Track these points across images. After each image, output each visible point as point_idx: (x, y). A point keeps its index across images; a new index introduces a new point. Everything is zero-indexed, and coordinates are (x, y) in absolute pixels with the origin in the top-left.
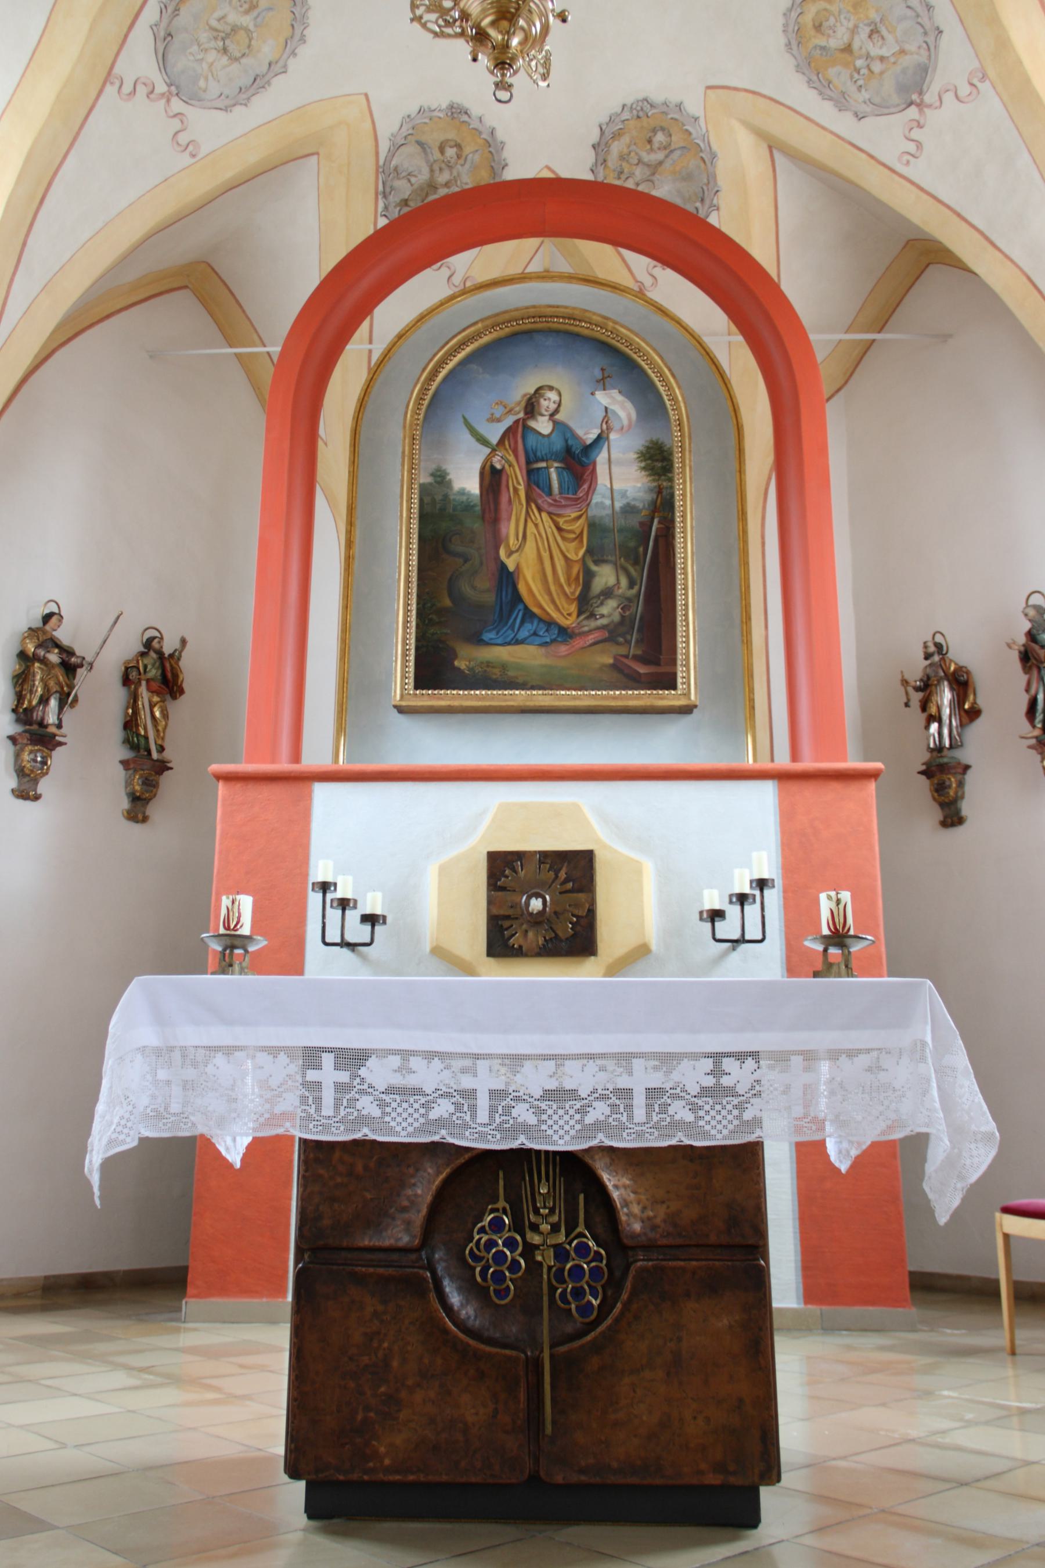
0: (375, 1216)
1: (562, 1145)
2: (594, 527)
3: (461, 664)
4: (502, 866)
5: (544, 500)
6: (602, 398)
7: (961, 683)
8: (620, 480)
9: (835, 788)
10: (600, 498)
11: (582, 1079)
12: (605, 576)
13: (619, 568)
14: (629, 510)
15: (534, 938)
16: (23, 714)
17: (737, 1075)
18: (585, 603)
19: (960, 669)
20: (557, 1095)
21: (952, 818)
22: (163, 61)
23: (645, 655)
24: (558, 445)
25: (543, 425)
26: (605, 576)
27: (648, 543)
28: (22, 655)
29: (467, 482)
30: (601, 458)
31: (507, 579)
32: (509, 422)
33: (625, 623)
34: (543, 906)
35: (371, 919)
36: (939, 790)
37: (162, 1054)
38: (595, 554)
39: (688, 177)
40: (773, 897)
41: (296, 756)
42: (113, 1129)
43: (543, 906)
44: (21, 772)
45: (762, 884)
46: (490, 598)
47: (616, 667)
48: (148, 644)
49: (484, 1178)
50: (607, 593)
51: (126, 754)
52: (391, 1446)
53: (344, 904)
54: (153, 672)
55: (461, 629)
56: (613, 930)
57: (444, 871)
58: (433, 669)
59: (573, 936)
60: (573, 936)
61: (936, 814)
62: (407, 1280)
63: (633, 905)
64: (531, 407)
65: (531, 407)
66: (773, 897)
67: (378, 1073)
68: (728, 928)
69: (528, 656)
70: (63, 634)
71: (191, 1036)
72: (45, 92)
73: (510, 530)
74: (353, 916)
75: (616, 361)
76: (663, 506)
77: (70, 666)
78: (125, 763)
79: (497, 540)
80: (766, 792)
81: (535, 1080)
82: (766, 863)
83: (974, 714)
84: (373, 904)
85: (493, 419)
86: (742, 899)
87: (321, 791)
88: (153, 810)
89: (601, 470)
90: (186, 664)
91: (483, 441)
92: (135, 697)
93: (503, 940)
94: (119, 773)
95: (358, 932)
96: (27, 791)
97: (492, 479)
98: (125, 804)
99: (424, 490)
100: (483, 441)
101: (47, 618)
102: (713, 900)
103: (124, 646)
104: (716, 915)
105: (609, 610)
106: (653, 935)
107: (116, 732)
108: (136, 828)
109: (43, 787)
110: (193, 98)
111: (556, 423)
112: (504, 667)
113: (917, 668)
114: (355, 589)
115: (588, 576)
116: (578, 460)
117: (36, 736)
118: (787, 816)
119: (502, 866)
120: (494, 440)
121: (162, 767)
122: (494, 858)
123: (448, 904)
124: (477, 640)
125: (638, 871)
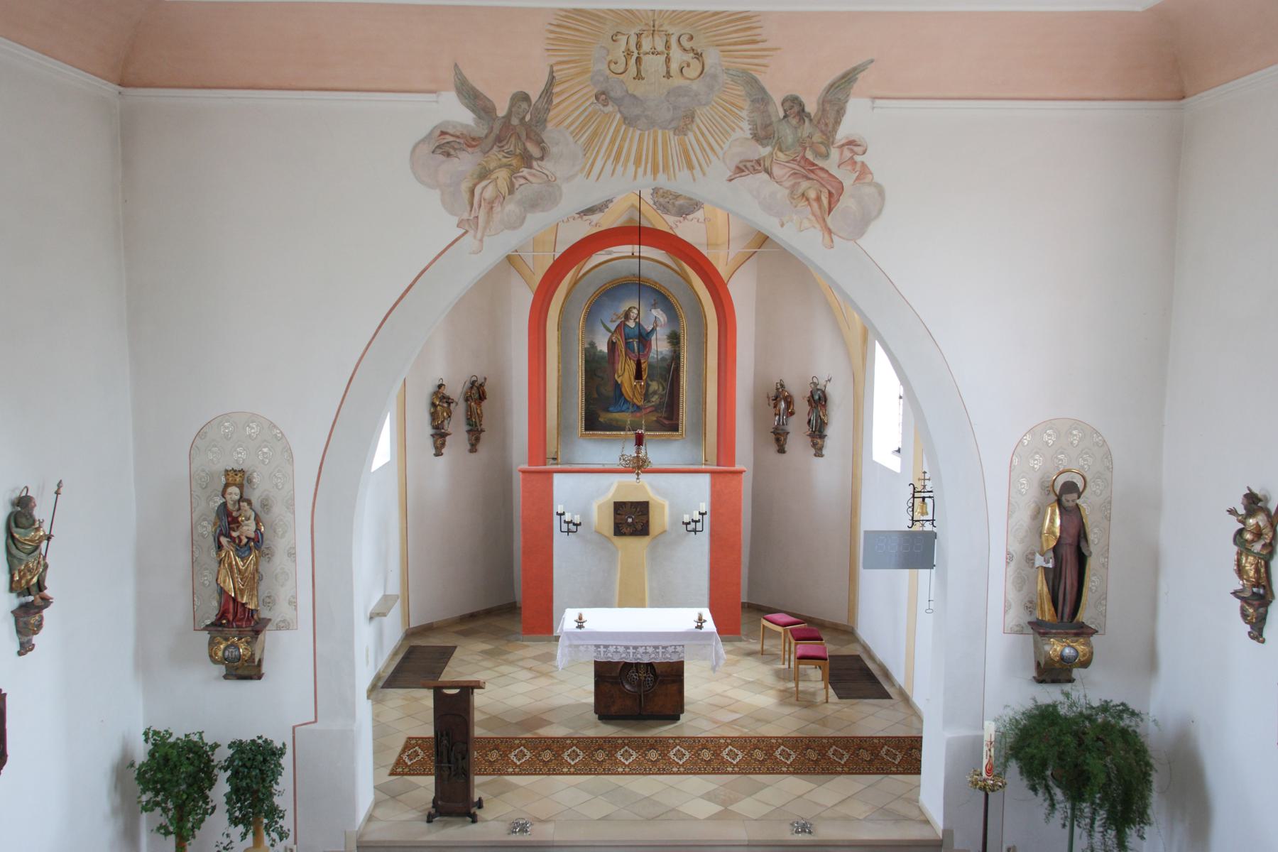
1: (646, 660)
3: (601, 420)
4: (619, 507)
6: (654, 312)
7: (789, 401)
8: (660, 347)
10: (653, 354)
12: (654, 386)
13: (659, 383)
14: (663, 359)
15: (629, 530)
17: (679, 649)
18: (646, 396)
19: (790, 396)
21: (781, 450)
23: (668, 420)
25: (631, 324)
26: (654, 386)
27: (671, 371)
28: (433, 405)
29: (603, 347)
30: (654, 338)
31: (618, 387)
32: (618, 322)
33: (661, 404)
34: (632, 519)
35: (577, 525)
36: (778, 440)
40: (707, 518)
43: (632, 519)
44: (436, 448)
45: (702, 514)
46: (611, 394)
47: (657, 421)
48: (473, 383)
50: (655, 393)
52: (614, 709)
56: (655, 526)
57: (600, 507)
58: (592, 423)
59: (641, 529)
60: (641, 529)
61: (774, 447)
63: (661, 519)
64: (627, 316)
65: (627, 316)
66: (707, 518)
67: (612, 649)
70: (447, 392)
71: (576, 643)
73: (619, 367)
75: (662, 299)
76: (676, 357)
78: (469, 432)
79: (614, 371)
80: (708, 476)
82: (705, 507)
83: (792, 414)
84: (577, 519)
87: (556, 477)
88: (479, 447)
89: (653, 343)
90: (486, 388)
91: (608, 330)
93: (619, 531)
94: (465, 436)
95: (574, 528)
96: (438, 453)
97: (612, 345)
98: (469, 447)
99: (586, 350)
100: (608, 330)
101: (440, 386)
102: (687, 519)
105: (655, 399)
106: (667, 527)
108: (473, 455)
111: (639, 324)
112: (617, 421)
113: (773, 393)
116: (644, 338)
117: (440, 437)
118: (713, 485)
119: (619, 507)
120: (613, 329)
121: (482, 431)
123: (601, 518)
124: (607, 411)
125: (663, 507)
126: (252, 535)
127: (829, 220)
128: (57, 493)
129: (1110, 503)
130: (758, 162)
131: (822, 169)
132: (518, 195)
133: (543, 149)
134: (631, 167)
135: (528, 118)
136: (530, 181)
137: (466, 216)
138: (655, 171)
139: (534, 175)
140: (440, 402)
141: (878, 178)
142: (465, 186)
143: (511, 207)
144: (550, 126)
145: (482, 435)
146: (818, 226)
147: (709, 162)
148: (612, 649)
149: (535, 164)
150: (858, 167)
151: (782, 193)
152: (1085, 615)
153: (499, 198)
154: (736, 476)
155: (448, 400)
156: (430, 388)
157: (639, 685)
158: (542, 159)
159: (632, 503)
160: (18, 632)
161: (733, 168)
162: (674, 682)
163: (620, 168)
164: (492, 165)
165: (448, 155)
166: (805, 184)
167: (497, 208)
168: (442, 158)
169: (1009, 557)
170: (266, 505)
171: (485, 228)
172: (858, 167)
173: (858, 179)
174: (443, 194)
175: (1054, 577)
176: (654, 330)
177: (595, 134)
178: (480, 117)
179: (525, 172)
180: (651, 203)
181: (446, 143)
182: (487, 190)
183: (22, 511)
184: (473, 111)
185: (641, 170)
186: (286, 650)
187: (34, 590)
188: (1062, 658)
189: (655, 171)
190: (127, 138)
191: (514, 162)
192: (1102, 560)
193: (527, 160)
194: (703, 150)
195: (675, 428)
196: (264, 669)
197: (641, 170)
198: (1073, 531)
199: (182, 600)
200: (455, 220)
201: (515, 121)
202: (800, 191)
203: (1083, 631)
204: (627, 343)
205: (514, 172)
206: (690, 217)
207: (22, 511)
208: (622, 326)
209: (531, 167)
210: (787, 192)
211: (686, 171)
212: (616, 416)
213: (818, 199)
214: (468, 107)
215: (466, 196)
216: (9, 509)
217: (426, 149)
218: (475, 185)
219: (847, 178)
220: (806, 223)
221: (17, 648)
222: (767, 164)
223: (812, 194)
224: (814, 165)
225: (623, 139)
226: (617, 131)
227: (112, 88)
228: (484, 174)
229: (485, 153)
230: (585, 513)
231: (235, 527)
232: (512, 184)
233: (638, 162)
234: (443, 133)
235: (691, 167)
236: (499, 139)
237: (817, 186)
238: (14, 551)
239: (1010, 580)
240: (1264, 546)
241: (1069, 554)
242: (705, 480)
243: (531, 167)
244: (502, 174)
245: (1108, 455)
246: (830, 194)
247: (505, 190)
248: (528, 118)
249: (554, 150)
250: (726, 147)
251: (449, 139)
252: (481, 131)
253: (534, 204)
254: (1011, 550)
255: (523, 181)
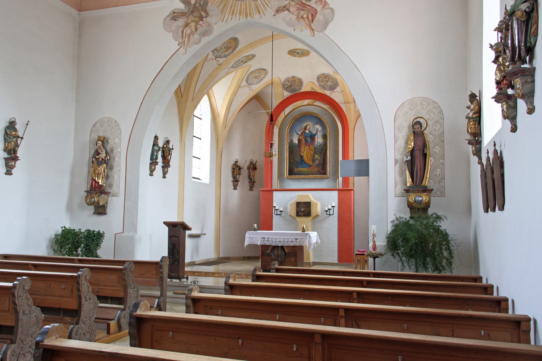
0: (267, 250)
2: (315, 148)
3: (295, 171)
4: (298, 204)
5: (307, 144)
6: (316, 126)
8: (319, 140)
9: (346, 191)
11: (282, 240)
12: (317, 156)
13: (319, 155)
14: (320, 145)
15: (302, 214)
16: (234, 177)
18: (313, 161)
20: (280, 241)
22: (247, 82)
23: (322, 171)
24: (309, 134)
25: (307, 131)
26: (317, 156)
27: (323, 150)
28: (233, 168)
29: (296, 141)
31: (302, 157)
34: (304, 209)
37: (249, 238)
38: (315, 153)
39: (333, 82)
41: (271, 187)
42: (246, 243)
43: (304, 209)
45: (333, 207)
46: (299, 160)
48: (251, 163)
49: (275, 247)
50: (317, 159)
51: (249, 180)
53: (277, 210)
54: (252, 167)
55: (296, 167)
56: (313, 213)
58: (291, 172)
62: (269, 255)
63: (318, 208)
65: (305, 128)
66: (336, 209)
67: (266, 239)
68: (328, 213)
69: (305, 169)
70: (238, 164)
71: (252, 236)
72: (231, 91)
73: (302, 149)
74: (278, 211)
75: (319, 120)
76: (325, 144)
77: (240, 169)
79: (300, 151)
80: (336, 193)
81: (278, 240)
85: (300, 131)
86: (329, 209)
87: (275, 193)
88: (254, 188)
89: (316, 139)
91: (298, 134)
92: (250, 171)
93: (298, 214)
95: (280, 213)
96: (235, 188)
97: (299, 140)
101: (236, 162)
103: (248, 163)
104: (327, 211)
105: (317, 162)
107: (247, 177)
108: (251, 192)
109: (237, 187)
110: (252, 84)
111: (309, 131)
114: (277, 162)
115: (314, 156)
116: (313, 137)
117: (236, 181)
119: (298, 204)
121: (254, 182)
122: (297, 203)
123: (292, 211)
124: (297, 167)
125: (317, 204)
126: (103, 158)
127: (312, 25)
128: (27, 124)
129: (443, 134)
130: (284, 7)
131: (309, 5)
132: (198, 32)
133: (207, 14)
134: (238, 16)
135: (202, 3)
136: (203, 26)
137: (181, 41)
138: (246, 17)
139: (204, 23)
140: (236, 169)
141: (331, 6)
142: (181, 30)
143: (196, 36)
144: (209, 5)
145: (255, 184)
146: (308, 28)
147: (266, 9)
148: (266, 239)
149: (204, 19)
150: (323, 3)
151: (294, 17)
152: (426, 182)
153: (192, 33)
154: (349, 192)
155: (240, 168)
156: (233, 162)
157: (278, 257)
158: (206, 17)
159: (304, 203)
160: (6, 166)
161: (275, 11)
162: (293, 256)
163: (234, 17)
164: (190, 21)
165: (175, 20)
166: (302, 13)
167: (191, 37)
168: (173, 21)
169: (396, 161)
170: (112, 151)
171: (187, 45)
172: (323, 3)
173: (323, 7)
174: (173, 34)
175: (411, 165)
176: (316, 133)
177: (225, 5)
178: (186, 5)
179: (201, 23)
180: (318, 85)
181: (175, 16)
182: (188, 31)
183: (12, 125)
184: (184, 3)
185: (241, 17)
186: (115, 205)
187: (12, 152)
188: (415, 201)
189: (246, 17)
190: (80, 28)
191: (197, 19)
192: (441, 161)
193: (201, 18)
194: (264, 5)
195: (325, 173)
196: (108, 210)
197: (241, 17)
198: (420, 144)
199: (84, 186)
200: (177, 43)
201: (198, 5)
202: (301, 16)
203: (426, 190)
204: (305, 139)
205: (197, 23)
206: (335, 90)
207: (12, 125)
208: (303, 133)
209: (202, 20)
210: (295, 17)
211: (258, 15)
212: (301, 169)
213: (308, 17)
214: (182, 2)
215: (180, 34)
216: (8, 124)
217: (168, 19)
218: (184, 29)
219: (319, 7)
220: (303, 28)
221: (5, 171)
222: (288, 7)
223: (305, 16)
224: (305, 4)
225: (235, 6)
226: (233, 3)
227: (74, 12)
228: (187, 25)
229: (187, 17)
230: (285, 208)
231: (101, 157)
232: (196, 27)
233: (240, 14)
234: (174, 13)
235: (259, 13)
236: (192, 12)
237: (307, 12)
238: (6, 137)
239: (397, 172)
240: (474, 113)
241: (418, 154)
242: (336, 193)
243: (202, 20)
244: (193, 24)
245: (441, 112)
246: (312, 14)
247: (194, 30)
248: (202, 3)
249: (210, 13)
250: (272, 3)
251: (176, 14)
252: (186, 10)
253: (204, 34)
254: (397, 158)
255: (200, 26)
